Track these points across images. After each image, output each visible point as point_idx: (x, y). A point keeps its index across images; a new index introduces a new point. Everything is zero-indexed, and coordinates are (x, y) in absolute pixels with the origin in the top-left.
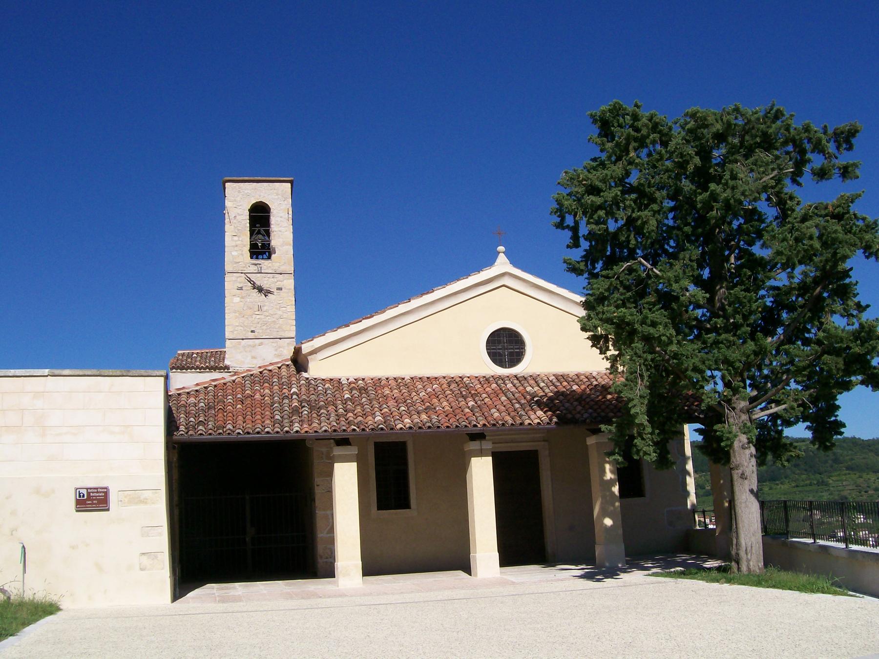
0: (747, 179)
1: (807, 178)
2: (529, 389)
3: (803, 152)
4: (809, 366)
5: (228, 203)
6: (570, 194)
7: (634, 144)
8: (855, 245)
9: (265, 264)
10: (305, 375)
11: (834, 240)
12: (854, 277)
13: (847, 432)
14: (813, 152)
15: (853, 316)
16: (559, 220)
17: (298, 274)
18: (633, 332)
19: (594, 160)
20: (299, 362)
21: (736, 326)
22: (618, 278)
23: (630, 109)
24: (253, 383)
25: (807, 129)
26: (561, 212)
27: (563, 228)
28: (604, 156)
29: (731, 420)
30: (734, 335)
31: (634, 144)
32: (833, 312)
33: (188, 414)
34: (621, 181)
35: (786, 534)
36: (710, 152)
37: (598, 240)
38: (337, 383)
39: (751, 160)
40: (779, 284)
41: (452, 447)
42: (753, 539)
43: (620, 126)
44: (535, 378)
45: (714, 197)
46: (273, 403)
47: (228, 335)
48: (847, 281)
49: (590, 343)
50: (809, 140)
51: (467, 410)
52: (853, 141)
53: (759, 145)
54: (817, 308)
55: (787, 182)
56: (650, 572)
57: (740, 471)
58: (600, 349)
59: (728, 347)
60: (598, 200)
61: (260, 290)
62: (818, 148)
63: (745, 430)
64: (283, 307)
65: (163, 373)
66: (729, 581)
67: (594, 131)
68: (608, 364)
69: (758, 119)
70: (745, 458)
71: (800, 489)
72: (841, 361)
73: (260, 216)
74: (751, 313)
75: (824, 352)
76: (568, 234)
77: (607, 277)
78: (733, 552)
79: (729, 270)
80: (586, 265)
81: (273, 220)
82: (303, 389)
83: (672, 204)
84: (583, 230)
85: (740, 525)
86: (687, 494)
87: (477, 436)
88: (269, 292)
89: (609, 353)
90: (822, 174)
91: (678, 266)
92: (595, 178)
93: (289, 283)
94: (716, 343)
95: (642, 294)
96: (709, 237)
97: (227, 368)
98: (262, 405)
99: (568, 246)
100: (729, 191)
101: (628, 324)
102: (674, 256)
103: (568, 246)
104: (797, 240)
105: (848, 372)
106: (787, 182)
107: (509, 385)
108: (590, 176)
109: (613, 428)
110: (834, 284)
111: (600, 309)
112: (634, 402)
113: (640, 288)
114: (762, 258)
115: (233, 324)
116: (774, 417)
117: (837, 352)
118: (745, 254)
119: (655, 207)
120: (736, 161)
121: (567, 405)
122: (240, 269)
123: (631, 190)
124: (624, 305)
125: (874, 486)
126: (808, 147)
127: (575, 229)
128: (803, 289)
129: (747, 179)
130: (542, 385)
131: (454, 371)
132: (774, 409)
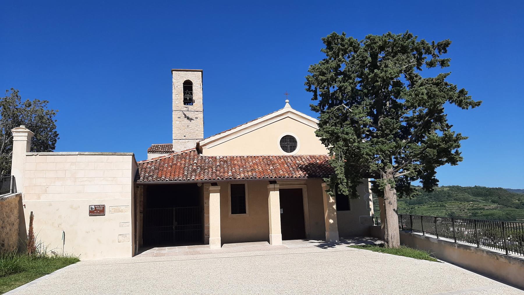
0: (392, 67)
1: (424, 66)
2: (297, 162)
3: (420, 54)
4: (420, 153)
5: (174, 80)
6: (313, 76)
7: (341, 52)
8: (444, 97)
9: (190, 107)
10: (201, 155)
11: (434, 95)
12: (445, 112)
13: (440, 184)
14: (425, 53)
15: (446, 130)
16: (308, 87)
17: (205, 111)
18: (338, 137)
19: (324, 60)
20: (199, 149)
21: (387, 135)
22: (333, 113)
23: (340, 35)
24: (178, 158)
25: (423, 43)
26: (309, 84)
27: (310, 91)
28: (328, 58)
29: (385, 177)
30: (386, 139)
31: (341, 52)
32: (435, 129)
33: (145, 172)
34: (336, 69)
35: (411, 230)
36: (377, 55)
37: (326, 96)
38: (214, 159)
39: (395, 58)
40: (409, 116)
41: (263, 185)
42: (395, 232)
43: (335, 44)
44: (301, 157)
45: (376, 75)
46: (185, 167)
47: (173, 138)
48: (442, 114)
49: (321, 142)
50: (424, 48)
51: (269, 171)
52: (447, 48)
53: (399, 51)
54: (427, 127)
55: (415, 68)
56: (349, 245)
57: (389, 201)
58: (325, 144)
59: (382, 145)
60: (324, 78)
61: (188, 118)
62: (428, 51)
63: (390, 182)
64: (198, 126)
65: (132, 154)
66: (383, 251)
67: (324, 47)
68: (329, 152)
69: (399, 39)
70: (391, 195)
71: (432, 208)
72: (435, 151)
73: (188, 86)
74: (394, 129)
75: (428, 147)
76: (312, 94)
77: (328, 113)
78: (386, 238)
79: (386, 109)
80: (320, 108)
81: (194, 88)
82: (199, 161)
83: (359, 80)
84: (319, 92)
85: (389, 226)
86: (370, 209)
87: (273, 182)
88: (192, 119)
89: (329, 147)
90: (431, 64)
91: (360, 108)
92: (323, 68)
93: (201, 115)
94: (377, 143)
95: (345, 119)
96: (377, 94)
97: (173, 152)
98: (180, 168)
99: (312, 99)
100: (383, 73)
101: (336, 133)
102: (359, 103)
103: (312, 99)
104: (417, 95)
105: (439, 156)
106: (415, 68)
107: (289, 160)
108: (321, 67)
109: (329, 180)
110: (436, 115)
111: (325, 127)
112: (338, 168)
113: (345, 117)
114: (401, 104)
115: (176, 133)
116: (406, 177)
117: (434, 147)
118: (394, 102)
119: (351, 81)
120: (388, 59)
121: (313, 169)
122: (179, 109)
123: (341, 73)
124: (335, 125)
125: (467, 208)
126: (423, 51)
127: (315, 92)
128: (420, 117)
129: (392, 67)
130: (304, 160)
131: (266, 154)
132: (406, 173)
